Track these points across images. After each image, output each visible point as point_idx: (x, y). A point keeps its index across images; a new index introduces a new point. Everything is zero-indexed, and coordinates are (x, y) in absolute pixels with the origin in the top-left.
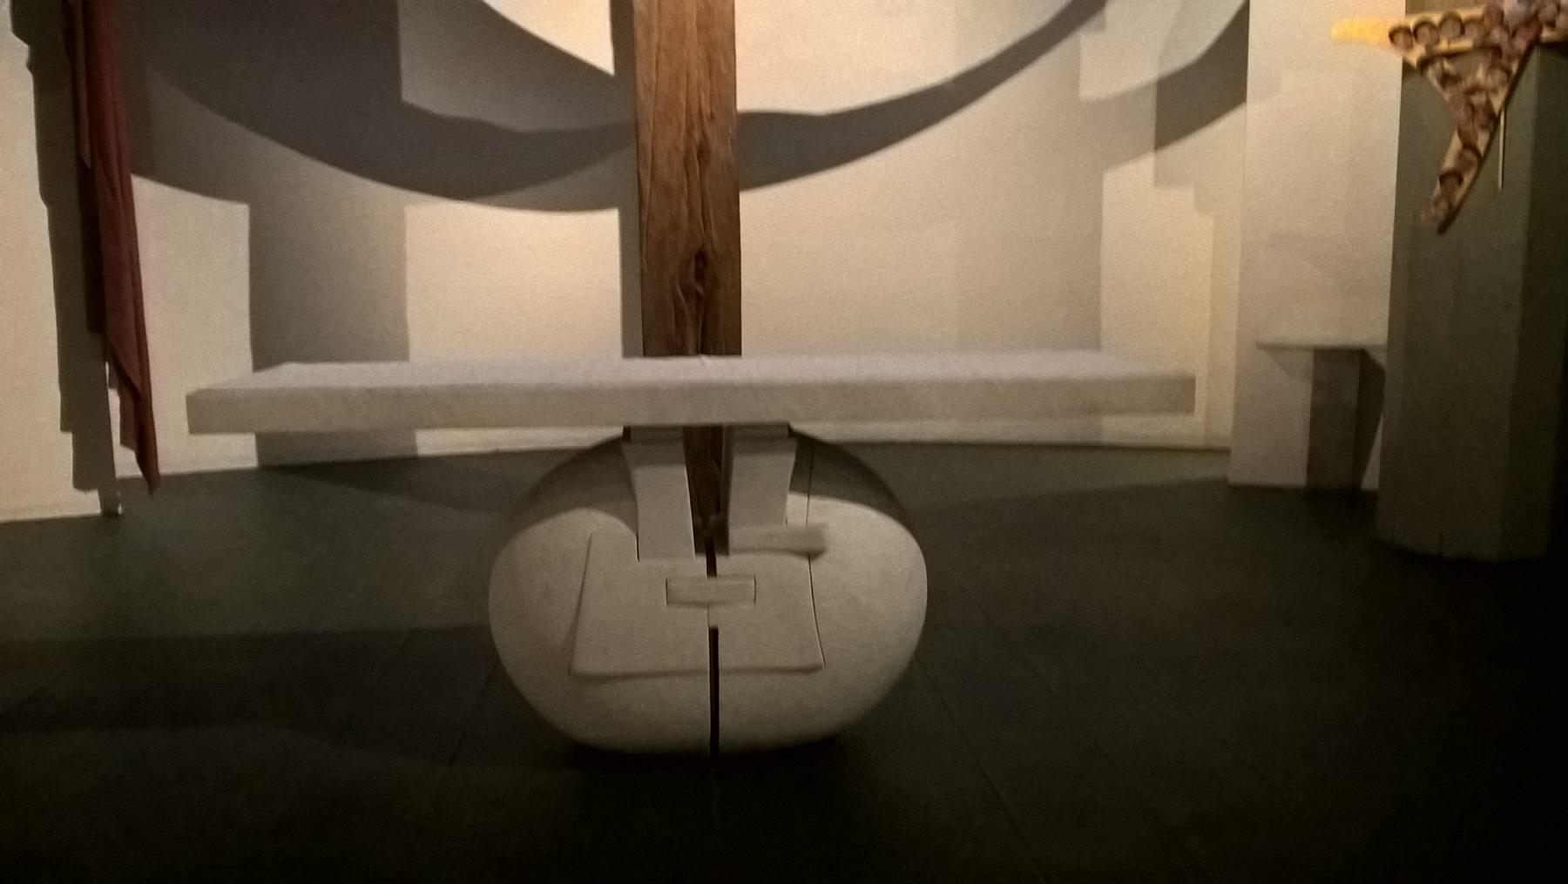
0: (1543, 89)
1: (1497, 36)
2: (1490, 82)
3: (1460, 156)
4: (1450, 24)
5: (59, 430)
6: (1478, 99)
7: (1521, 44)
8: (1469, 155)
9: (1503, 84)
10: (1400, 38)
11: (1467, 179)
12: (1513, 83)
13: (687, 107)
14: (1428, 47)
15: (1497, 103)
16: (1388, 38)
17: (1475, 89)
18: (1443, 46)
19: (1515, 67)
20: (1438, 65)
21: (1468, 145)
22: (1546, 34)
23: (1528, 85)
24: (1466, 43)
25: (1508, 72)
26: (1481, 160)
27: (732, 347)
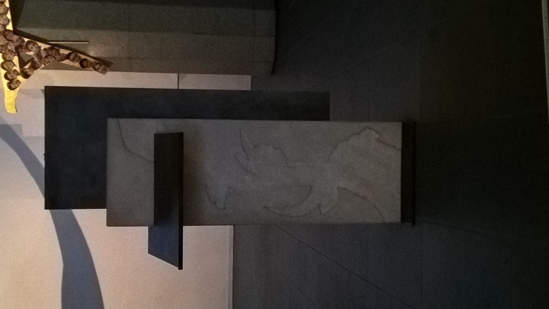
0: (38, 24)
1: (12, 47)
2: (34, 49)
3: (72, 61)
4: (5, 66)
5: (182, 270)
6: (43, 54)
7: (15, 37)
8: (72, 57)
9: (34, 44)
10: (13, 86)
11: (83, 57)
12: (35, 39)
13: (100, 61)
14: (18, 74)
15: (43, 46)
16: (12, 91)
17: (38, 55)
18: (17, 68)
19: (26, 40)
20: (28, 71)
21: (68, 57)
22: (10, 27)
23: (35, 32)
24: (16, 60)
25: (28, 43)
26: (74, 51)
27: (159, 138)
